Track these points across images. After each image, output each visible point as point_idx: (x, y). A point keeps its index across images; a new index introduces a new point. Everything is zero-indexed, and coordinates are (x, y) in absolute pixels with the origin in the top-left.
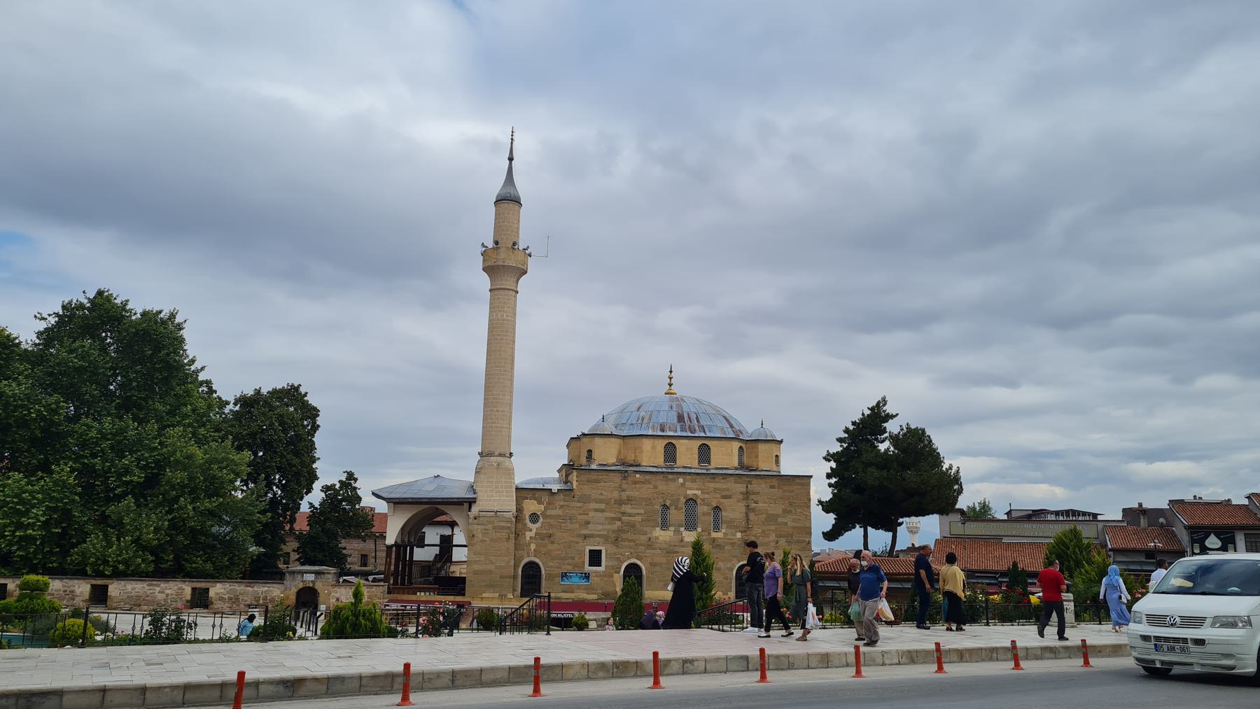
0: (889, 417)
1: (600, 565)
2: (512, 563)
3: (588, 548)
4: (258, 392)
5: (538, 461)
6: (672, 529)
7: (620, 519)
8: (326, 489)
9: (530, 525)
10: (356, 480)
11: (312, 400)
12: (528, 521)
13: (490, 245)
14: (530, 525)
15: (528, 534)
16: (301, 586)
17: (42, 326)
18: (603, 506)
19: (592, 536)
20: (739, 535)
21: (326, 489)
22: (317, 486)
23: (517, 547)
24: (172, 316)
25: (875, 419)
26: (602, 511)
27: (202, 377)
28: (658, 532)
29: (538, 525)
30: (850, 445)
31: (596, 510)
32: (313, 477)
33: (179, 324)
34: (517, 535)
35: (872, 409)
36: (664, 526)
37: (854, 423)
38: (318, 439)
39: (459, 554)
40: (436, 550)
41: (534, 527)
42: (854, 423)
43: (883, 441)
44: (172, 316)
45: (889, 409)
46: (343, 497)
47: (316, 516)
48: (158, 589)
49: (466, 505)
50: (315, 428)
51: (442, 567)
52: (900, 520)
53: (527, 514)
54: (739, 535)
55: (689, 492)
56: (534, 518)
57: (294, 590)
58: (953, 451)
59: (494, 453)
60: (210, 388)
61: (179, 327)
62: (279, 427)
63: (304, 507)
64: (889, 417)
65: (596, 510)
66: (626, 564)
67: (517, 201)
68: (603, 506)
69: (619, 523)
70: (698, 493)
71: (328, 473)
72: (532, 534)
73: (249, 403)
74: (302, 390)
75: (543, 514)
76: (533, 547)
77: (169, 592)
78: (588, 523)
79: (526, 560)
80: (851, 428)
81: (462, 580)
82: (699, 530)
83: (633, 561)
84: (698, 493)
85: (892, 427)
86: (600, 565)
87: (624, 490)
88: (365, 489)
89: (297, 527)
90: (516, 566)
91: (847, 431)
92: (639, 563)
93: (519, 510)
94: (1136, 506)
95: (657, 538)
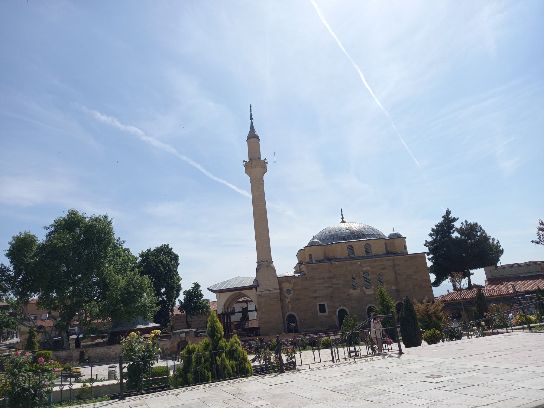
0: (455, 220)
1: (325, 312)
2: (282, 316)
3: (318, 304)
4: (149, 250)
5: (285, 265)
6: (359, 288)
7: (331, 287)
8: (186, 293)
9: (287, 295)
10: (199, 286)
11: (175, 251)
12: (285, 293)
13: (248, 160)
14: (287, 295)
15: (287, 300)
16: (179, 340)
17: (48, 232)
18: (322, 281)
19: (319, 297)
20: (394, 288)
21: (186, 293)
22: (181, 293)
23: (282, 307)
24: (106, 217)
25: (448, 221)
26: (322, 283)
27: (125, 246)
28: (352, 291)
29: (291, 295)
30: (437, 237)
31: (319, 284)
32: (179, 288)
33: (109, 222)
34: (282, 301)
35: (444, 217)
36: (355, 288)
37: (436, 226)
38: (179, 270)
39: (252, 316)
40: (241, 315)
41: (289, 296)
42: (436, 226)
43: (453, 233)
44: (106, 217)
45: (452, 216)
46: (194, 294)
47: (183, 307)
48: (111, 350)
49: (254, 289)
50: (178, 264)
51: (245, 324)
52: (471, 271)
53: (285, 290)
54: (394, 288)
55: (364, 269)
56: (289, 292)
57: (176, 343)
58: (493, 231)
59: (265, 263)
60: (129, 252)
61: (110, 223)
62: (161, 265)
63: (177, 304)
64: (455, 220)
65: (319, 284)
66: (338, 310)
67: (257, 137)
68: (322, 281)
69: (331, 289)
70: (369, 268)
71: (186, 285)
72: (289, 300)
73: (145, 256)
74: (170, 247)
75: (293, 288)
76: (290, 306)
77: (117, 351)
78: (315, 291)
79: (288, 314)
80: (435, 228)
81: (258, 328)
82: (373, 287)
83: (342, 307)
84: (369, 268)
85: (457, 225)
86: (325, 312)
87: (331, 272)
88: (203, 290)
89: (175, 313)
90: (283, 317)
91: (433, 230)
92: (345, 308)
93: (281, 288)
94: (447, 293)
95: (352, 294)
